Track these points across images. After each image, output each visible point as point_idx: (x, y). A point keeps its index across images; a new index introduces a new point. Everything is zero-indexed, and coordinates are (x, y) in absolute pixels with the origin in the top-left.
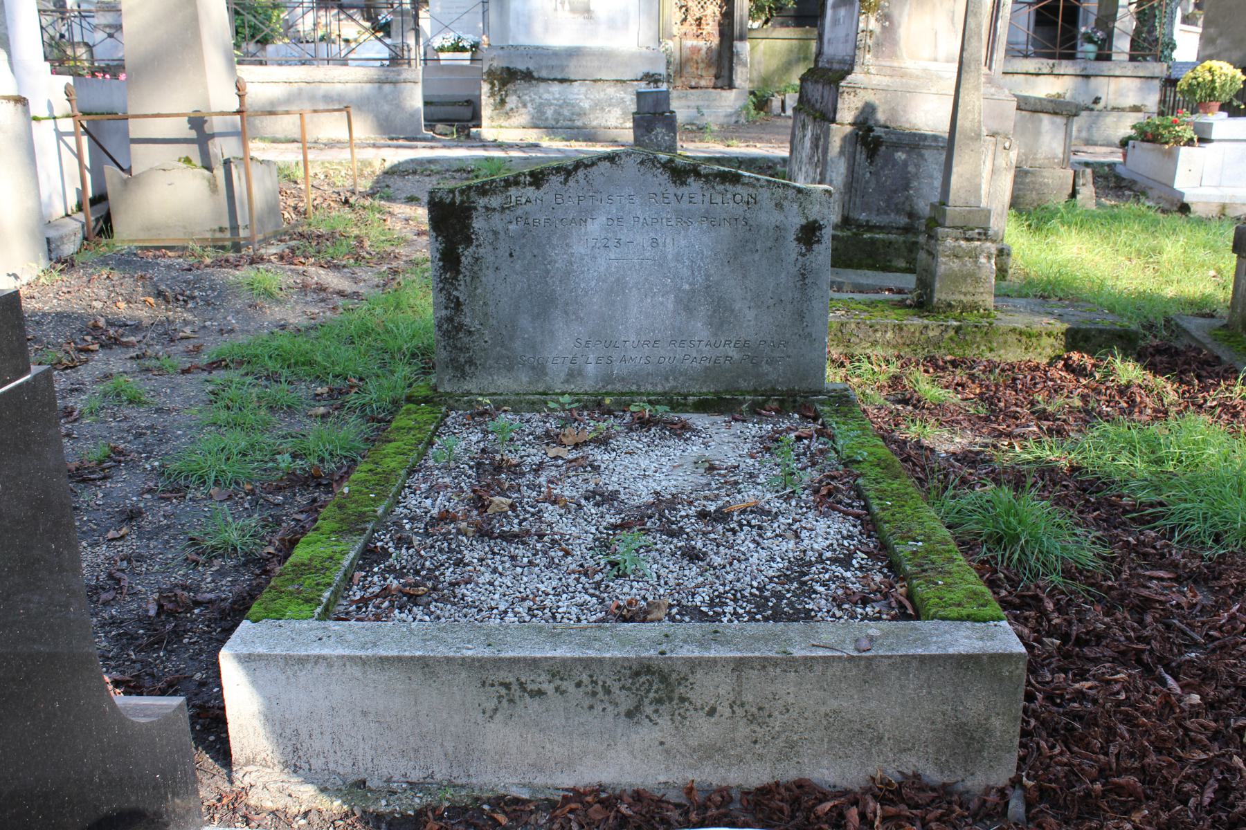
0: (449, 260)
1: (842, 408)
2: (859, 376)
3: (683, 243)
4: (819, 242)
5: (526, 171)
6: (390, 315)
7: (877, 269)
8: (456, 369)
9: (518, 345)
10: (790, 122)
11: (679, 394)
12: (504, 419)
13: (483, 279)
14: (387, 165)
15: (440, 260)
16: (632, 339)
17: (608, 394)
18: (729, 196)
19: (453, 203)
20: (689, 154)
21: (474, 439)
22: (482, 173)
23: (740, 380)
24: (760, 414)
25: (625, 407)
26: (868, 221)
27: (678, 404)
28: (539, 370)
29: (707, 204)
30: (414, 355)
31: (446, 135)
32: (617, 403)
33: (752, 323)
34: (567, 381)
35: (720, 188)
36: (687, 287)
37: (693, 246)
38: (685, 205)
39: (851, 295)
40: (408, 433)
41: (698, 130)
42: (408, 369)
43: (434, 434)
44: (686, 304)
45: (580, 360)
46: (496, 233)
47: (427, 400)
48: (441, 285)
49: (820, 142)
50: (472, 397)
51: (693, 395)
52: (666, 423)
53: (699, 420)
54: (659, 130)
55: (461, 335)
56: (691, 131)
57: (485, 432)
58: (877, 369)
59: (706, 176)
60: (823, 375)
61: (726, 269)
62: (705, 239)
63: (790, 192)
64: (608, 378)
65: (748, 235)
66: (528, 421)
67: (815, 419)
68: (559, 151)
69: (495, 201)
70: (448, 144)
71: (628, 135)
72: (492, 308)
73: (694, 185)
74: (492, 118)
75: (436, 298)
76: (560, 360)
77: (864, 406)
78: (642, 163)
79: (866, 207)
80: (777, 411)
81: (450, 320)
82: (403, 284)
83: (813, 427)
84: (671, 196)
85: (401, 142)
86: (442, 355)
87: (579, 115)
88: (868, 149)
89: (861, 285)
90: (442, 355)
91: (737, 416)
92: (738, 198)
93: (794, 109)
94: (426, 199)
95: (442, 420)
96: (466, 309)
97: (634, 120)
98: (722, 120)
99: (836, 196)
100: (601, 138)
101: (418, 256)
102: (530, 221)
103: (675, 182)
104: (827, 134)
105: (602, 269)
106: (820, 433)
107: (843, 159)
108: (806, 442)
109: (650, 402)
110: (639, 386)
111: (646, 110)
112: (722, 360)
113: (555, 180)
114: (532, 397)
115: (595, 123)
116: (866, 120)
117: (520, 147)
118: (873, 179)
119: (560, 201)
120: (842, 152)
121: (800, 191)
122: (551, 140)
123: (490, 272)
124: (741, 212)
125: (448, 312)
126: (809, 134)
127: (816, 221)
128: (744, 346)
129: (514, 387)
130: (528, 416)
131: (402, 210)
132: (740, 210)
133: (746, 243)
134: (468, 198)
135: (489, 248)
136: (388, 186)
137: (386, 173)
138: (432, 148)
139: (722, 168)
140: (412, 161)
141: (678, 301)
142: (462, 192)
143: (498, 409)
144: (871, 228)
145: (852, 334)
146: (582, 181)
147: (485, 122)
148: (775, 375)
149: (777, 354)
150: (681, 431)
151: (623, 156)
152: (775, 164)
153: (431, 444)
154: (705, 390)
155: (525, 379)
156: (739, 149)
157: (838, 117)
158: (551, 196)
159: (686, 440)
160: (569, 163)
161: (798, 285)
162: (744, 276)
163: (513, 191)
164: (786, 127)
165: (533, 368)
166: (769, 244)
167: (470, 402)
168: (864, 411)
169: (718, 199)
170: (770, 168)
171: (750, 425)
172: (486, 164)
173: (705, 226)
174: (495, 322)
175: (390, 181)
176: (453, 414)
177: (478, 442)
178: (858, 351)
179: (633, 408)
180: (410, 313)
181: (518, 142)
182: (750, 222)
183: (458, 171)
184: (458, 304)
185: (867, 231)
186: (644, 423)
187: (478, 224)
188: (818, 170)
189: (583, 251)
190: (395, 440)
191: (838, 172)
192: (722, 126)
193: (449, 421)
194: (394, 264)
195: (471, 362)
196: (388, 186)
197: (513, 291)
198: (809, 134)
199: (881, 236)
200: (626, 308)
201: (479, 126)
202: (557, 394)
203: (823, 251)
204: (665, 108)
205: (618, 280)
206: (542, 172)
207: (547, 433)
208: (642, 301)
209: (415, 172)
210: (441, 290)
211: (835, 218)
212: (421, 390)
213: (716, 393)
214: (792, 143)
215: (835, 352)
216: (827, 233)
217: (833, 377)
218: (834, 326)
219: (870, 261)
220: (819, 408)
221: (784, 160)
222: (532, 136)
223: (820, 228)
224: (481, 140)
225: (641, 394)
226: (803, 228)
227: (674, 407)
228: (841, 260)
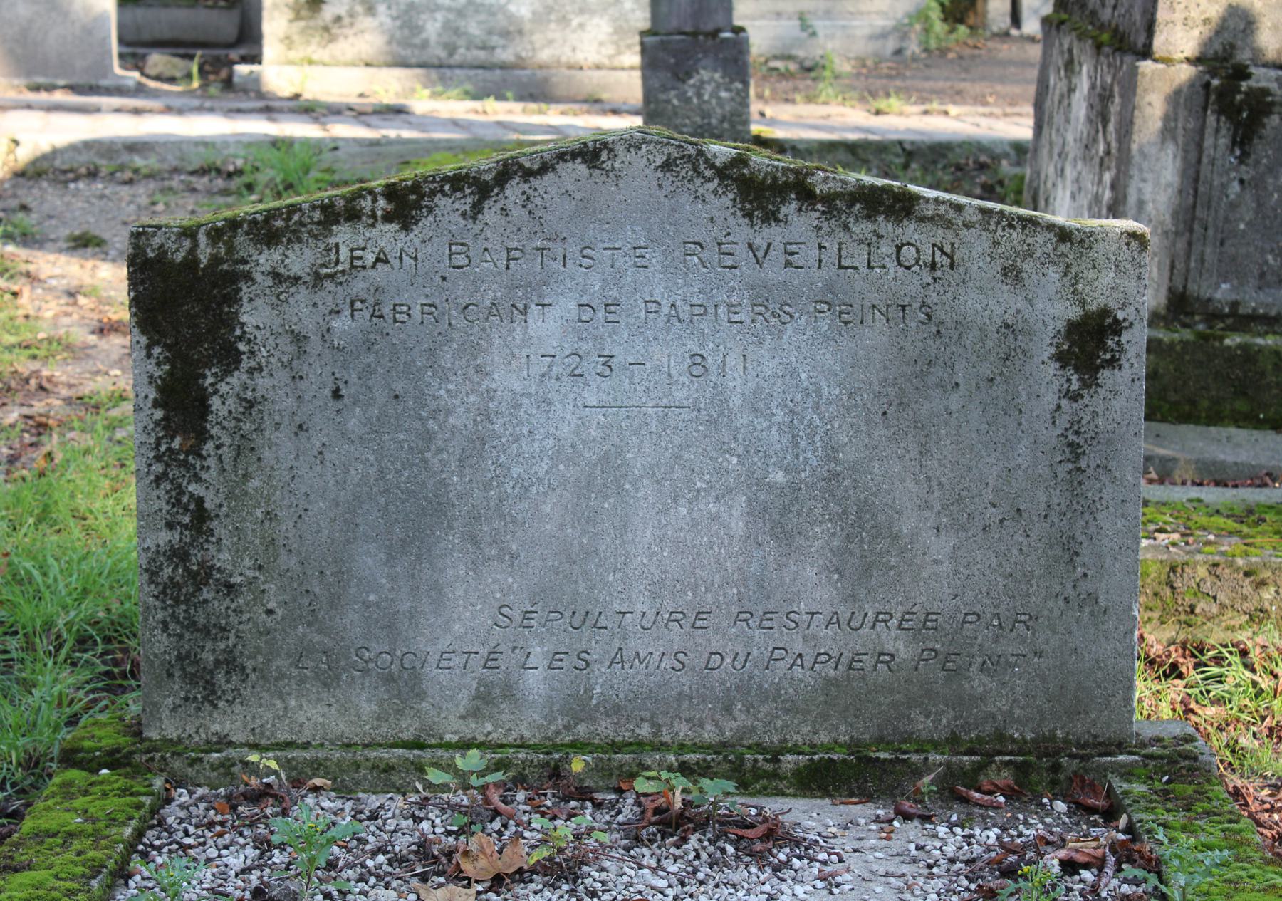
0: (181, 407)
1: (1178, 787)
2: (1219, 701)
3: (770, 365)
4: (1113, 363)
5: (378, 184)
6: (25, 537)
7: (1258, 424)
8: (192, 679)
9: (351, 620)
10: (1035, 52)
11: (759, 748)
12: (315, 810)
13: (266, 454)
14: (24, 155)
15: (156, 404)
16: (639, 608)
17: (578, 746)
18: (886, 248)
19: (191, 262)
20: (779, 134)
21: (235, 861)
22: (262, 178)
23: (916, 714)
24: (966, 801)
25: (621, 780)
26: (1235, 305)
27: (758, 774)
28: (404, 684)
29: (830, 271)
30: (83, 642)
31: (172, 80)
32: (602, 769)
33: (943, 567)
34: (475, 714)
35: (862, 228)
36: (779, 477)
37: (795, 373)
38: (774, 271)
39: (1194, 492)
40: (65, 845)
41: (804, 73)
42: (68, 679)
43: (131, 847)
44: (777, 519)
45: (508, 661)
46: (299, 339)
47: (115, 759)
48: (158, 468)
49: (1112, 107)
50: (232, 753)
51: (795, 750)
52: (726, 822)
53: (809, 815)
54: (705, 74)
55: (206, 594)
56: (785, 76)
57: (264, 846)
58: (1265, 683)
59: (828, 199)
60: (1128, 700)
61: (879, 432)
62: (825, 357)
63: (1042, 241)
64: (579, 707)
65: (933, 346)
66: (373, 817)
67: (1110, 815)
68: (455, 123)
69: (299, 260)
70: (177, 102)
71: (630, 86)
72: (285, 527)
73: (799, 223)
74: (288, 41)
75: (143, 499)
76: (457, 660)
77: (1234, 780)
78: (667, 166)
79: (1231, 269)
80: (1010, 794)
81: (179, 555)
82: (59, 457)
83: (1107, 835)
84: (741, 251)
85: (59, 97)
86: (155, 645)
87: (506, 34)
88: (1237, 124)
89: (1222, 465)
90: (155, 645)
91: (907, 805)
92: (908, 253)
93: (1046, 21)
94: (120, 241)
95: (154, 811)
96: (220, 529)
97: (644, 50)
98: (861, 48)
99: (1154, 242)
100: (561, 91)
101: (100, 386)
102: (387, 310)
103: (749, 215)
104: (1130, 86)
105: (566, 431)
106: (1125, 854)
107: (1171, 149)
108: (1087, 875)
109: (685, 769)
110: (657, 727)
111: (674, 24)
112: (868, 661)
113: (449, 208)
114: (384, 754)
115: (545, 55)
116: (1230, 48)
117: (358, 114)
118: (1249, 200)
119: (461, 260)
120: (1168, 131)
121: (1064, 235)
122: (434, 95)
123: (283, 437)
124: (915, 289)
125: (175, 536)
126: (1083, 84)
127: (1105, 312)
128: (922, 625)
129: (341, 727)
130: (374, 801)
131: (59, 267)
132: (913, 284)
133: (927, 367)
134: (231, 249)
135: (283, 376)
136: (24, 208)
137: (20, 174)
138: (137, 112)
139: (868, 179)
140: (88, 145)
141: (757, 511)
142: (215, 235)
143: (297, 783)
144: (1243, 321)
145: (1199, 591)
146: (517, 212)
147: (271, 48)
148: (1007, 702)
149: (1008, 648)
150: (765, 843)
151: (620, 149)
152: (996, 158)
153: (123, 874)
154: (824, 738)
155: (367, 707)
156: (906, 119)
157: (1158, 43)
158: (438, 248)
159: (776, 869)
160: (484, 163)
161: (1062, 471)
162: (924, 451)
163: (343, 235)
164: (1025, 64)
165: (389, 679)
166: (987, 369)
167: (226, 765)
168: (1237, 794)
169: (858, 257)
170: (982, 167)
171: (942, 830)
172: (273, 155)
173: (824, 325)
174: (293, 562)
175: (30, 195)
176: (182, 796)
177: (246, 870)
178: (1215, 636)
179: (641, 785)
180: (77, 532)
181: (353, 100)
182: (940, 314)
183: (202, 172)
184: (201, 516)
185: (1233, 329)
186: (672, 824)
187: (254, 314)
188: (1107, 177)
189: (518, 386)
190: (29, 867)
191: (1159, 180)
192: (862, 62)
193: (172, 815)
194: (38, 407)
195: (230, 663)
196: (24, 208)
197: (341, 484)
198: (1083, 84)
199: (1270, 341)
200: (624, 529)
201: (255, 59)
202: (449, 746)
203: (1126, 384)
204: (719, 20)
205: (605, 457)
206: (416, 188)
207: (423, 848)
208: (664, 512)
209: (93, 174)
210: (158, 480)
211: (1152, 297)
212: (101, 733)
213: (854, 746)
214: (1039, 106)
215: (1157, 638)
216: (1135, 340)
217: (1154, 704)
218: (1153, 570)
219: (1241, 405)
220: (1120, 785)
221: (1020, 149)
222: (389, 85)
223: (1117, 328)
224: (261, 95)
225: (661, 747)
226: (1074, 329)
227: (746, 780)
228: (1167, 404)
